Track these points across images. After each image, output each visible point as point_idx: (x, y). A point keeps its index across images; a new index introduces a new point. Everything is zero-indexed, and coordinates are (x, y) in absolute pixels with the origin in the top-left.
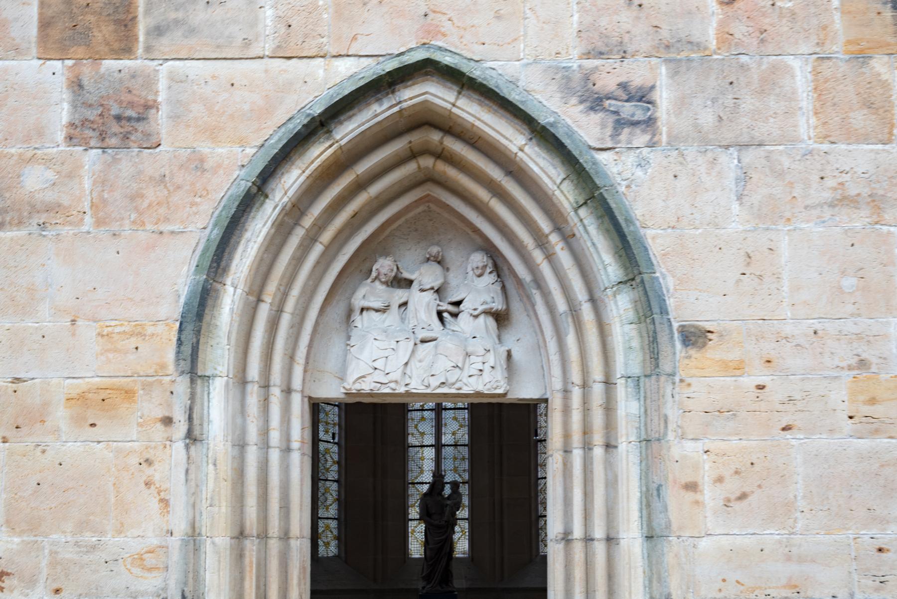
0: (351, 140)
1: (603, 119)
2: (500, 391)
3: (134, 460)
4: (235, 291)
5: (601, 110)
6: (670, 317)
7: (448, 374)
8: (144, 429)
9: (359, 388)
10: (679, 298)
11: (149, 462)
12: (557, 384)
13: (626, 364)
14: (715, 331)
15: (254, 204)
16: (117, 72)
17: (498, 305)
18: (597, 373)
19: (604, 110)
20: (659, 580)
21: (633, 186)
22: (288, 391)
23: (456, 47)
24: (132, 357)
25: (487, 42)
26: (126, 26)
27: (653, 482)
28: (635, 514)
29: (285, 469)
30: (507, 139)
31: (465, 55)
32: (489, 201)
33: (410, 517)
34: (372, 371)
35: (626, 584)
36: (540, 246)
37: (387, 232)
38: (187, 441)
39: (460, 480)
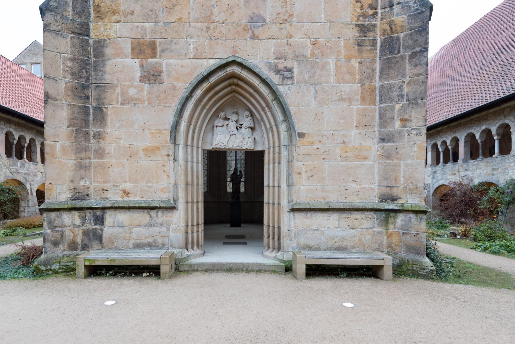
3: (160, 165)
6: (296, 130)
11: (164, 166)
12: (267, 147)
13: (284, 142)
17: (252, 125)
18: (277, 144)
19: (280, 74)
20: (290, 196)
22: (198, 148)
23: (241, 56)
25: (249, 55)
26: (154, 49)
28: (285, 180)
33: (228, 181)
35: (282, 197)
39: (242, 170)
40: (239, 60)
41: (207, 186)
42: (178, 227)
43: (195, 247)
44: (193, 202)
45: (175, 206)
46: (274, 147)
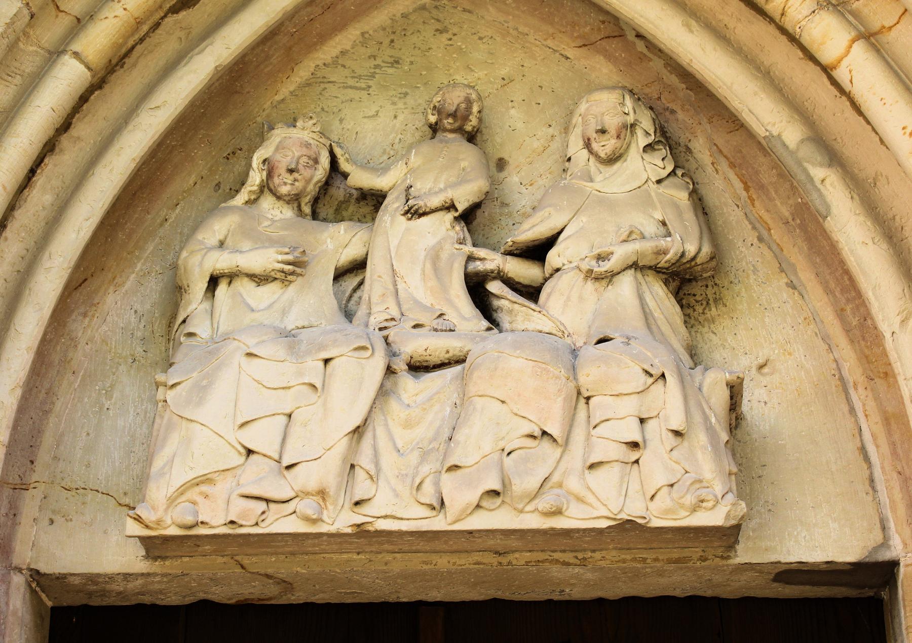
7: (508, 461)
9: (189, 519)
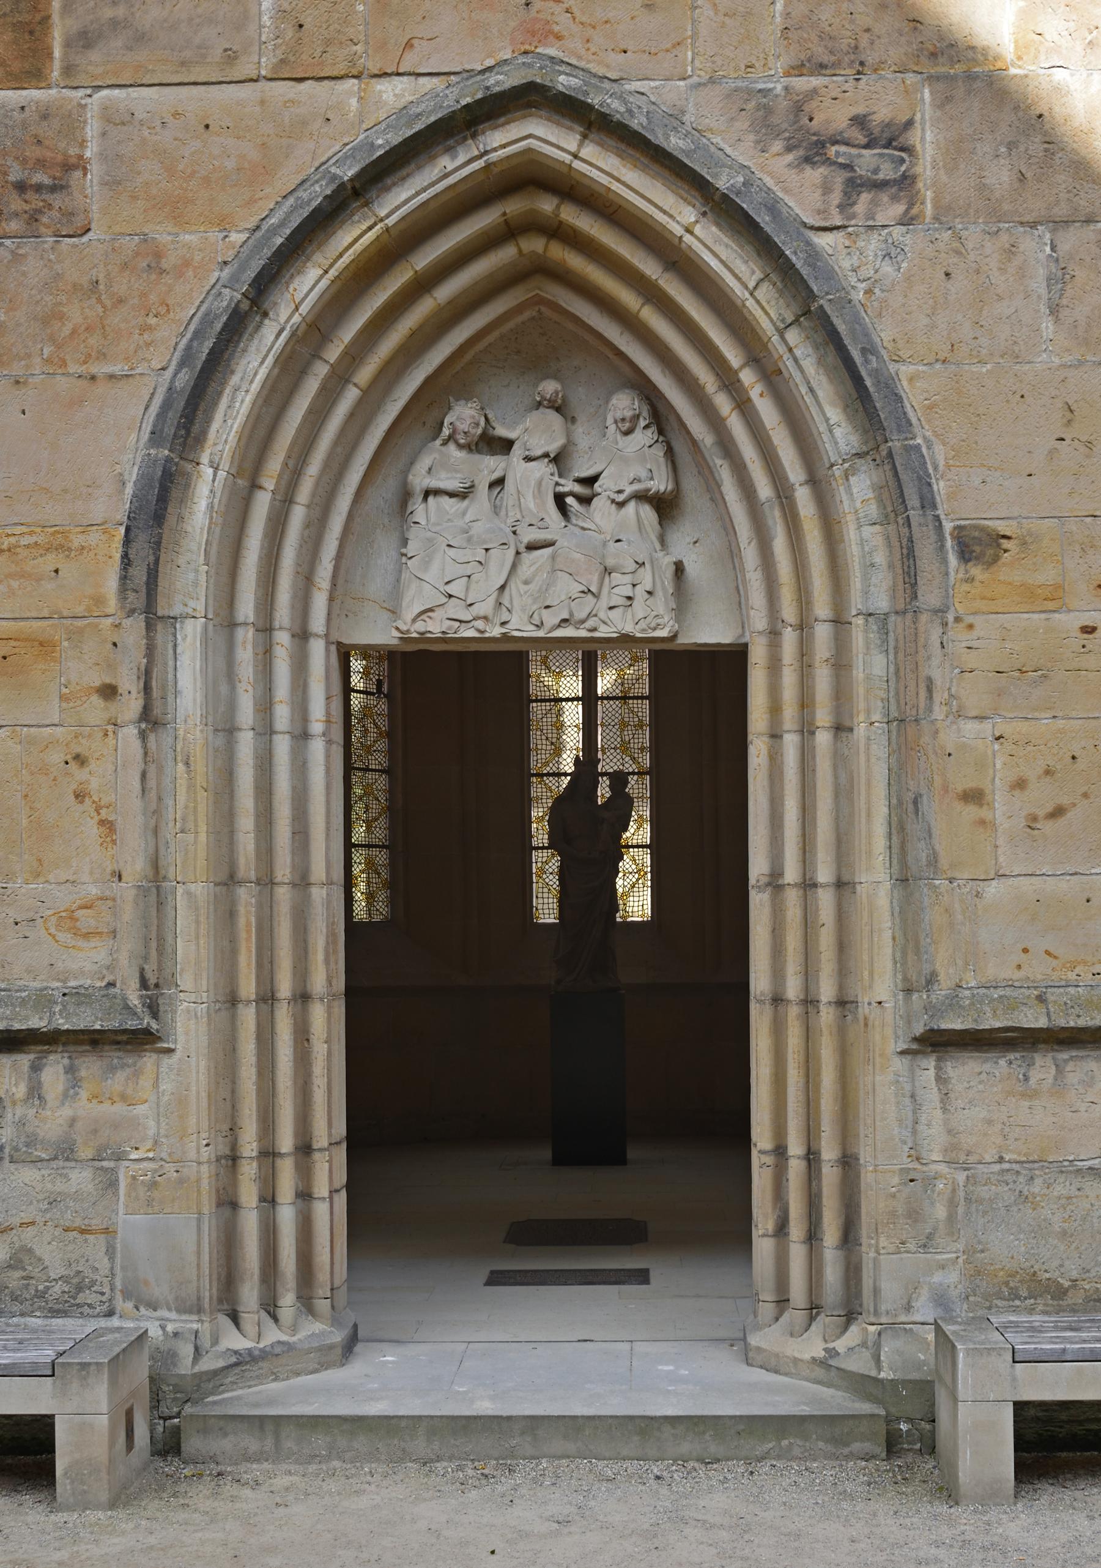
0: (403, 218)
1: (826, 177)
2: (663, 633)
3: (56, 757)
4: (215, 475)
5: (823, 163)
6: (939, 512)
7: (573, 604)
8: (71, 704)
9: (423, 630)
10: (954, 481)
11: (80, 760)
12: (759, 621)
13: (866, 593)
14: (1014, 536)
15: (245, 328)
16: (18, 110)
17: (660, 484)
18: (822, 608)
19: (829, 162)
20: (917, 952)
21: (877, 291)
22: (302, 636)
23: (580, 58)
24: (48, 586)
25: (630, 48)
26: (31, 33)
27: (908, 789)
28: (880, 843)
29: (300, 769)
30: (665, 212)
31: (593, 71)
32: (639, 311)
33: (534, 843)
34: (445, 600)
35: (865, 957)
36: (726, 386)
37: (469, 356)
38: (143, 726)
39: (630, 767)
40: (564, 82)
41: (391, 885)
42: (170, 1168)
43: (288, 1300)
44: (267, 998)
45: (154, 1026)
46: (804, 626)
